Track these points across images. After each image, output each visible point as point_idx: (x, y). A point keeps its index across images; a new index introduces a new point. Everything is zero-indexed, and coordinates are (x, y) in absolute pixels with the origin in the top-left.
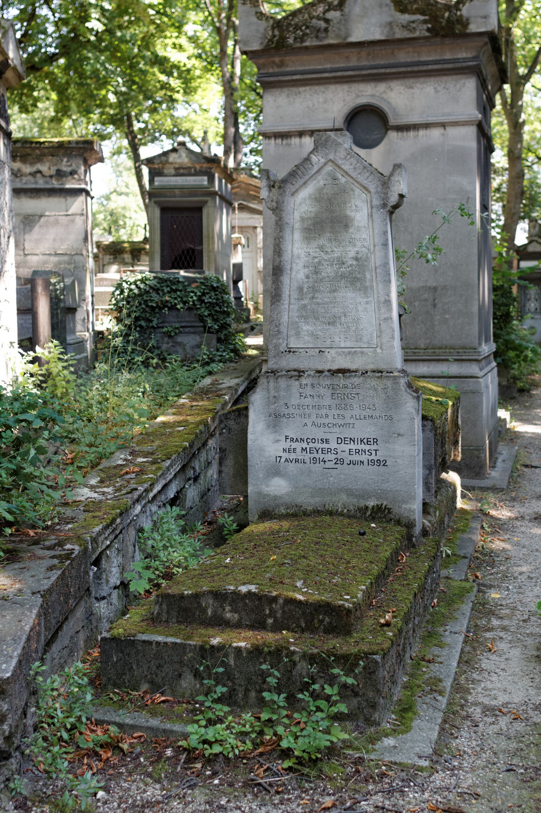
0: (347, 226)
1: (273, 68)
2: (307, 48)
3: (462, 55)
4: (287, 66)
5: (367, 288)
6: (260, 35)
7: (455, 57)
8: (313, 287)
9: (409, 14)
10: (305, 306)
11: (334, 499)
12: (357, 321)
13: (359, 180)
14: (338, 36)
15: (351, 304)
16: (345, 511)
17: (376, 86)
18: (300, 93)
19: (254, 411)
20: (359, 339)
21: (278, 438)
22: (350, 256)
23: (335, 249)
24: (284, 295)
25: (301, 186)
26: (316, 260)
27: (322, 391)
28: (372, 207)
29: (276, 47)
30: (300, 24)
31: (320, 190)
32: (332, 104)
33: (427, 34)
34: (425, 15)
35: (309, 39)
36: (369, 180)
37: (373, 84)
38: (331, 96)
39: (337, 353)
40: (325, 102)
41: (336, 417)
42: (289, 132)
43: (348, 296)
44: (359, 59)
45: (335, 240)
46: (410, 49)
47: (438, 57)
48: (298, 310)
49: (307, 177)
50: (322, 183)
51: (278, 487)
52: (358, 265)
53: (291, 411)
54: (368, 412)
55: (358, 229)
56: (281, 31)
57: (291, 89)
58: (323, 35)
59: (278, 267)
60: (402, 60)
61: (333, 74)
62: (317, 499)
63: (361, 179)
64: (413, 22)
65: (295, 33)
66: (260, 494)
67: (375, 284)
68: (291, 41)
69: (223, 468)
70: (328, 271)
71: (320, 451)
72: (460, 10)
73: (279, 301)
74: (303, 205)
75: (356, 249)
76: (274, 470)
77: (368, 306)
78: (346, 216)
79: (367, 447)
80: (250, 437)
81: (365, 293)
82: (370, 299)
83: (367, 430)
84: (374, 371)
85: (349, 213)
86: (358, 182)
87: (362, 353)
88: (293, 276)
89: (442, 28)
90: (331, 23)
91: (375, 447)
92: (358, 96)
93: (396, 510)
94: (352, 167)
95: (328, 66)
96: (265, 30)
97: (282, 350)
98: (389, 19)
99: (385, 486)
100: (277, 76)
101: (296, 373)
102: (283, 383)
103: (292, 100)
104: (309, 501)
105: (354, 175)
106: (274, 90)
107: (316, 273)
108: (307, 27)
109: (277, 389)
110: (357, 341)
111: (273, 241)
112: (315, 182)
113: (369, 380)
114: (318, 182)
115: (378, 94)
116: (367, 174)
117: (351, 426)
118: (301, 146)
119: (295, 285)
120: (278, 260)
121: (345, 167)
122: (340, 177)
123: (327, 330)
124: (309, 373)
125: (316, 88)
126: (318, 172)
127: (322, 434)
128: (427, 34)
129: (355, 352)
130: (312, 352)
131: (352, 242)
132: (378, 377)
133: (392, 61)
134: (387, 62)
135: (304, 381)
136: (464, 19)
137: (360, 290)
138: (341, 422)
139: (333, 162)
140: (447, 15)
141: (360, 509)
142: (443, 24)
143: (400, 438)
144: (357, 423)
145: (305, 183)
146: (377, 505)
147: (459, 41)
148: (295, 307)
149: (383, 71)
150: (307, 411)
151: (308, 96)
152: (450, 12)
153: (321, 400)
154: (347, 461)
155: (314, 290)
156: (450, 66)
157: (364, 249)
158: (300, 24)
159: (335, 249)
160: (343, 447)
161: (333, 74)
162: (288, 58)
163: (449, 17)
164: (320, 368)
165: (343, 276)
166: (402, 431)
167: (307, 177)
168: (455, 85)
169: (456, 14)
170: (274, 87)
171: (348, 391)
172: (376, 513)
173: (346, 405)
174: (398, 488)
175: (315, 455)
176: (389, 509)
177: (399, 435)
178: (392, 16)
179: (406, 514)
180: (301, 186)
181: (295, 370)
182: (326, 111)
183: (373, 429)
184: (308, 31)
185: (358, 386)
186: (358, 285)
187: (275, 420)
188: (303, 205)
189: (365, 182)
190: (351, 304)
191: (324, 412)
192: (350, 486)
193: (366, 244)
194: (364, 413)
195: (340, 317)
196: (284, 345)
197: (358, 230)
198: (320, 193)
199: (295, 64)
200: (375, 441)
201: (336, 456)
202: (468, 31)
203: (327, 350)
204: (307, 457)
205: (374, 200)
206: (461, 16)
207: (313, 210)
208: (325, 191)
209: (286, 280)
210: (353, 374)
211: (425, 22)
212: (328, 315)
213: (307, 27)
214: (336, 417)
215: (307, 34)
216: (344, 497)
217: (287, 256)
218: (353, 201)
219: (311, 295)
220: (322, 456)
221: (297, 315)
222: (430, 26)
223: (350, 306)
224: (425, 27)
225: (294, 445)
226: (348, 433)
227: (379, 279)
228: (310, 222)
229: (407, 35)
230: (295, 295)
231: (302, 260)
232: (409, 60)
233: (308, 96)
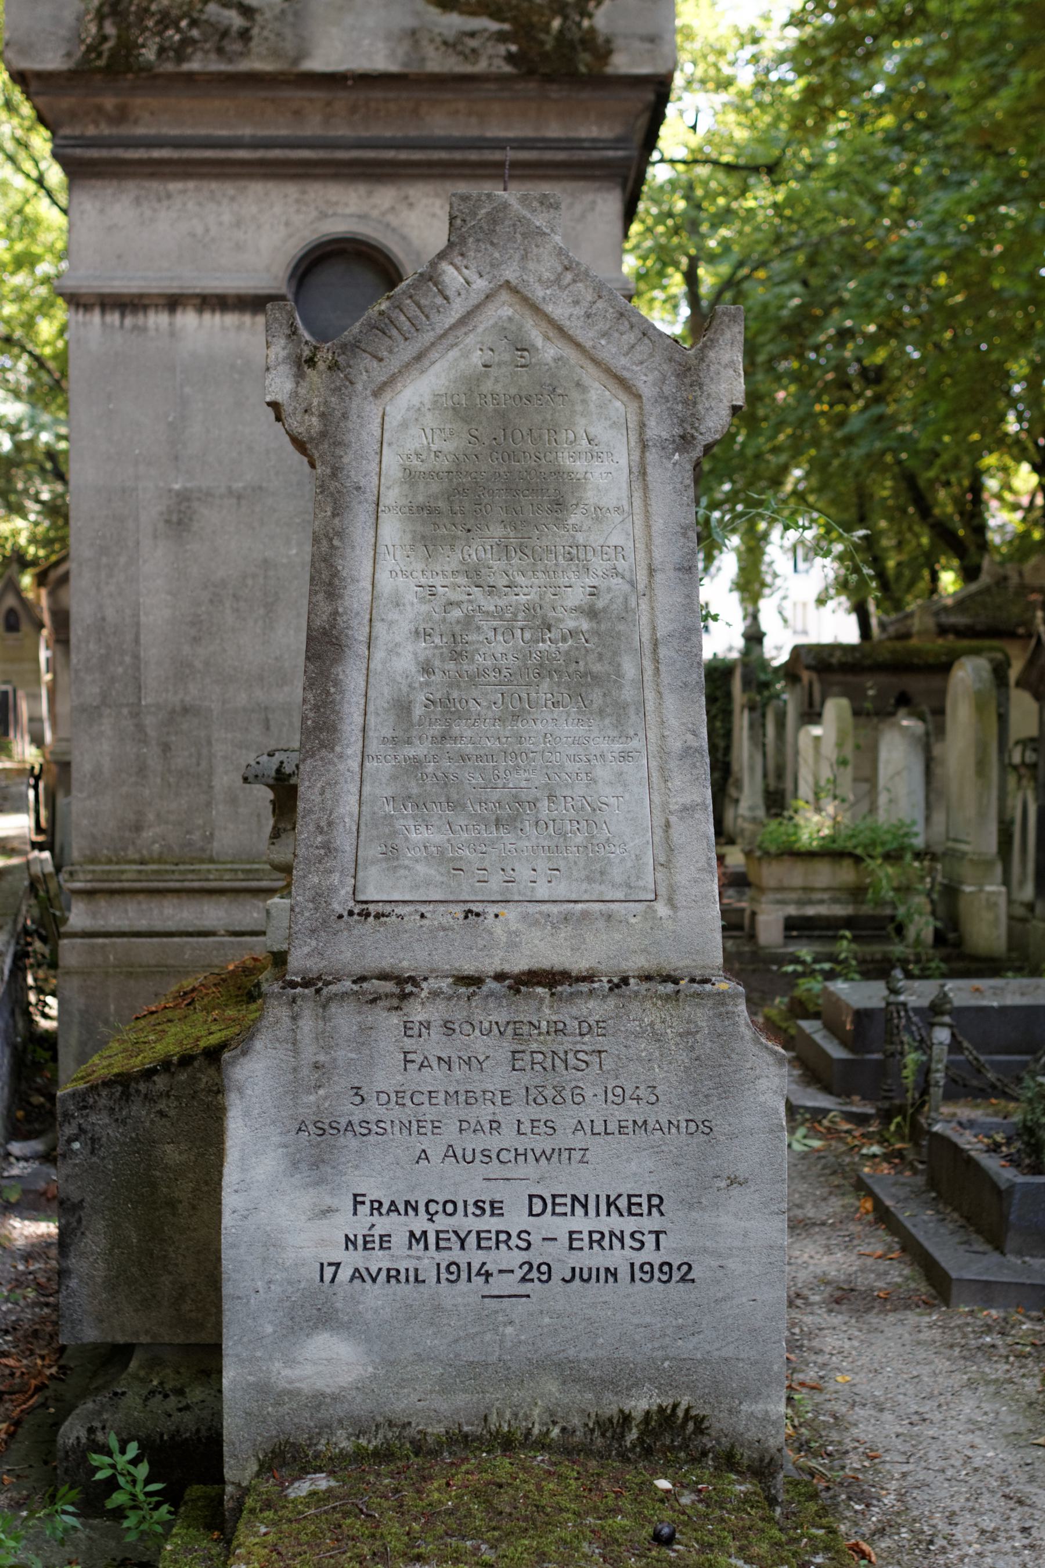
0: (559, 505)
1: (96, 124)
2: (190, 77)
3: (589, 131)
4: (136, 122)
5: (625, 707)
6: (63, 32)
7: (572, 134)
8: (446, 702)
9: (462, 13)
10: (416, 764)
11: (517, 1395)
12: (590, 814)
14: (276, 53)
15: (574, 758)
16: (556, 1432)
17: (370, 194)
18: (169, 196)
19: (247, 1114)
20: (598, 874)
21: (329, 1201)
22: (570, 603)
23: (520, 579)
25: (407, 366)
26: (456, 613)
27: (479, 1044)
29: (108, 66)
30: (175, 12)
31: (471, 383)
32: (260, 231)
33: (507, 69)
34: (503, 20)
35: (199, 55)
37: (362, 188)
38: (254, 209)
40: (238, 224)
41: (526, 1127)
42: (141, 296)
43: (561, 733)
44: (327, 120)
45: (521, 548)
46: (461, 106)
47: (529, 132)
48: (394, 778)
49: (428, 337)
50: (477, 358)
51: (328, 1365)
53: (374, 1110)
54: (634, 1111)
55: (598, 515)
56: (123, 26)
57: (147, 184)
58: (237, 47)
59: (325, 633)
60: (439, 132)
61: (259, 154)
62: (461, 1399)
64: (472, 35)
65: (160, 34)
66: (263, 1389)
67: (650, 695)
68: (149, 54)
69: (72, 1262)
70: (495, 649)
71: (472, 1240)
72: (590, 16)
73: (329, 746)
74: (415, 430)
76: (316, 1309)
77: (628, 767)
78: (558, 473)
79: (629, 1224)
80: (231, 1200)
82: (635, 744)
83: (630, 1169)
84: (648, 978)
85: (566, 462)
86: (596, 362)
87: (609, 917)
88: (376, 664)
89: (545, 56)
90: (258, 17)
91: (654, 1222)
92: (323, 216)
93: (720, 1422)
94: (579, 311)
95: (247, 131)
96: (79, 19)
97: (338, 908)
98: (410, 22)
99: (685, 1347)
100: (110, 146)
101: (389, 987)
102: (345, 1019)
103: (148, 213)
104: (430, 1405)
105: (586, 336)
106: (99, 183)
107: (456, 656)
108: (194, 23)
109: (326, 1040)
110: (589, 879)
111: (308, 548)
112: (453, 354)
113: (635, 1007)
114: (466, 355)
116: (631, 337)
117: (577, 1155)
118: (173, 334)
119: (382, 694)
120: (325, 609)
121: (558, 311)
122: (539, 342)
123: (493, 843)
124: (433, 983)
125: (214, 185)
126: (463, 321)
127: (479, 1184)
128: (507, 69)
129: (585, 915)
130: (439, 916)
131: (576, 556)
132: (667, 998)
133: (413, 133)
134: (399, 134)
135: (418, 1012)
136: (600, 40)
137: (601, 712)
138: (543, 1143)
139: (514, 290)
140: (556, 23)
141: (604, 1425)
142: (548, 47)
143: (735, 1191)
144: (597, 1146)
145: (419, 357)
146: (661, 1409)
147: (585, 95)
148: (380, 768)
149: (390, 154)
150: (429, 1112)
151: (190, 205)
152: (566, 18)
153: (475, 1075)
154: (561, 1271)
155: (448, 709)
156: (561, 156)
157: (616, 581)
158: (175, 12)
159: (520, 579)
160: (559, 1226)
161: (259, 154)
162: (139, 101)
163: (561, 31)
164: (469, 968)
165: (544, 669)
166: (742, 1170)
167: (428, 337)
169: (579, 25)
170: (99, 175)
171: (566, 1043)
172: (656, 1434)
173: (559, 1090)
174: (729, 1352)
175: (456, 1254)
176: (699, 1421)
177: (733, 1181)
178: (417, 14)
179: (752, 1434)
180: (407, 366)
181: (384, 977)
182: (239, 247)
183: (649, 1164)
184: (195, 33)
185: (586, 1028)
186: (596, 696)
187: (319, 1142)
188: (415, 430)
189: (622, 363)
190: (574, 758)
191: (484, 1112)
192: (571, 1352)
193: (622, 565)
194: (619, 1113)
196: (345, 891)
198: (470, 393)
199: (157, 119)
200: (656, 1203)
201: (524, 1256)
202: (609, 70)
203: (492, 909)
204: (427, 1261)
205: (652, 423)
206: (592, 30)
207: (449, 446)
208: (488, 386)
210: (584, 987)
211: (501, 37)
212: (495, 795)
213: (194, 23)
214: (526, 1127)
215: (193, 42)
216: (551, 1387)
217: (356, 598)
218: (582, 421)
219: (437, 729)
220: (477, 1257)
221: (389, 792)
222: (514, 48)
223: (570, 766)
224: (502, 49)
225: (383, 1224)
226: (567, 1180)
227: (665, 678)
228: (435, 487)
229: (453, 65)
230: (382, 727)
232: (456, 133)
233: (190, 205)
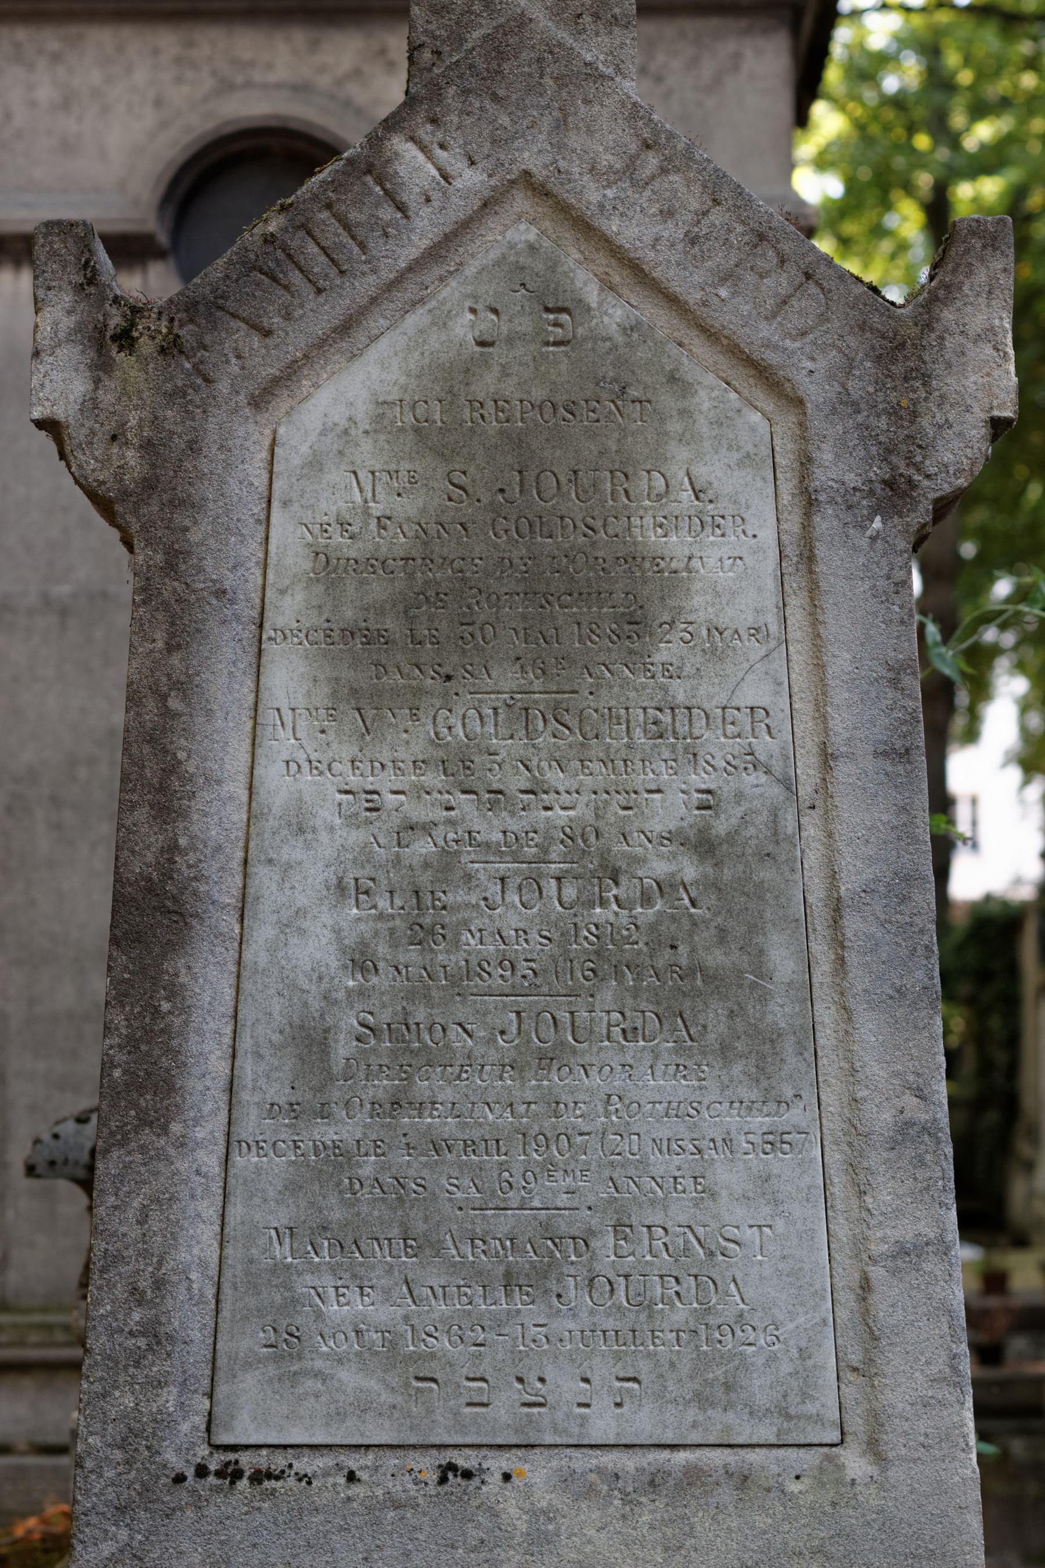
0: (635, 625)
5: (774, 1038)
10: (340, 1157)
12: (704, 1263)
13: (724, 319)
15: (668, 1146)
17: (314, 45)
23: (554, 777)
24: (193, 1084)
25: (322, 344)
26: (423, 847)
28: (809, 502)
31: (452, 379)
36: (795, 321)
37: (299, 36)
38: (96, 77)
39: (566, 1479)
40: (66, 103)
43: (641, 1094)
45: (557, 714)
48: (293, 1187)
49: (366, 286)
50: (464, 328)
52: (714, 886)
55: (717, 643)
63: (735, 311)
67: (826, 1014)
70: (504, 920)
74: (336, 475)
75: (699, 779)
77: (780, 1163)
81: (762, 1072)
82: (796, 1116)
86: (710, 334)
87: (743, 1480)
88: (256, 953)
92: (226, 87)
105: (688, 283)
110: (702, 1400)
112: (415, 320)
114: (442, 321)
115: (324, 81)
119: (269, 1013)
121: (630, 231)
122: (592, 294)
123: (499, 1324)
126: (435, 253)
129: (693, 1475)
130: (386, 1478)
131: (671, 729)
137: (725, 1051)
139: (541, 192)
145: (345, 328)
148: (264, 1167)
155: (406, 1045)
159: (554, 777)
165: (606, 961)
167: (366, 286)
168: (694, 63)
180: (322, 344)
182: (68, 147)
186: (715, 1018)
188: (336, 475)
189: (761, 335)
190: (668, 1146)
193: (765, 745)
195: (585, 1239)
197: (714, 654)
205: (826, 455)
207: (408, 507)
209: (206, 978)
212: (504, 1223)
217: (216, 818)
218: (681, 454)
219: (383, 1086)
221: (281, 1217)
223: (660, 1163)
227: (858, 979)
228: (378, 590)
230: (267, 1082)
231: (326, 846)
